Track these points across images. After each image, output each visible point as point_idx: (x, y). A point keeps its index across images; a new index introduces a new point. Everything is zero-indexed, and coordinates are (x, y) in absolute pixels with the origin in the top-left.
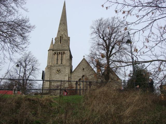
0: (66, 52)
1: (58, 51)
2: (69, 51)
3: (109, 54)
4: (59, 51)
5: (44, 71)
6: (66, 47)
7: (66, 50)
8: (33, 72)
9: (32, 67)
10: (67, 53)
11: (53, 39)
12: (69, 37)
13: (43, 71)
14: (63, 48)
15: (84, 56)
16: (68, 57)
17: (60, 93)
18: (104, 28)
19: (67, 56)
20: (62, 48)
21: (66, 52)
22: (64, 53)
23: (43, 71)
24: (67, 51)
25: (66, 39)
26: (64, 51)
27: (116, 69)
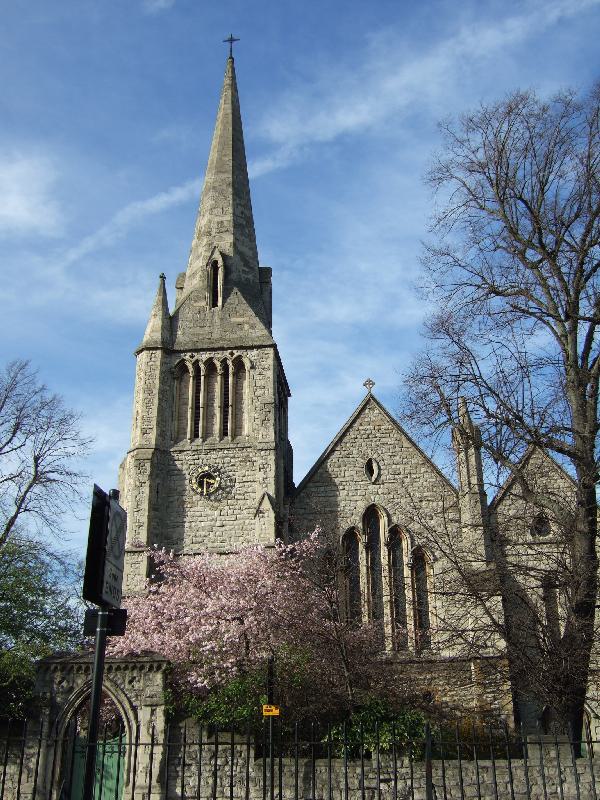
0: (249, 357)
1: (197, 356)
2: (271, 351)
3: (58, 770)
4: (205, 356)
5: (107, 489)
6: (253, 327)
7: (252, 348)
8: (37, 489)
9: (36, 459)
10: (256, 390)
11: (163, 277)
12: (266, 273)
13: (98, 493)
14: (234, 337)
15: (369, 383)
16: (269, 394)
17: (487, 600)
18: (495, 182)
19: (262, 383)
20: (229, 336)
21: (249, 357)
22: (239, 364)
23: (98, 493)
24: (255, 352)
25: (250, 276)
26: (237, 353)
27: (528, 493)
